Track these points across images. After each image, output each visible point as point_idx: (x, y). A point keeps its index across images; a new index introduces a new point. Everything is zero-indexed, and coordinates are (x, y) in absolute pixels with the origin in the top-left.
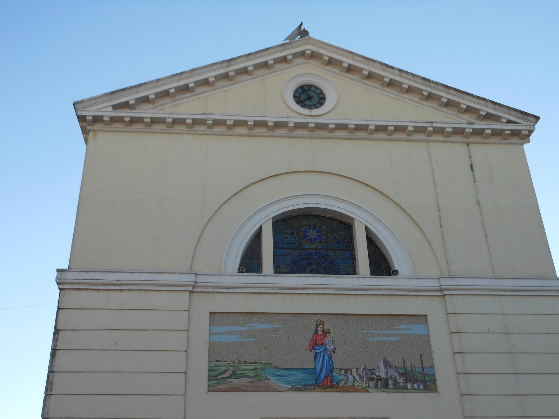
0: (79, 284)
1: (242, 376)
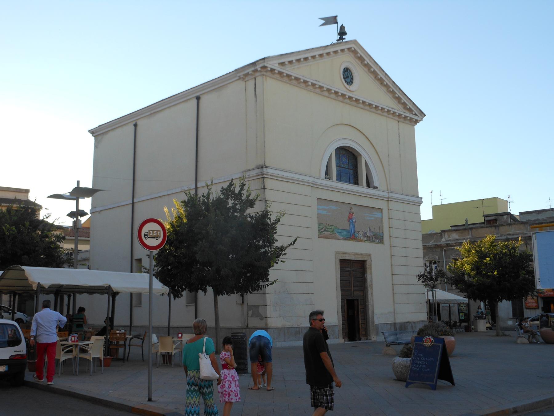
0: (273, 176)
1: (328, 231)
